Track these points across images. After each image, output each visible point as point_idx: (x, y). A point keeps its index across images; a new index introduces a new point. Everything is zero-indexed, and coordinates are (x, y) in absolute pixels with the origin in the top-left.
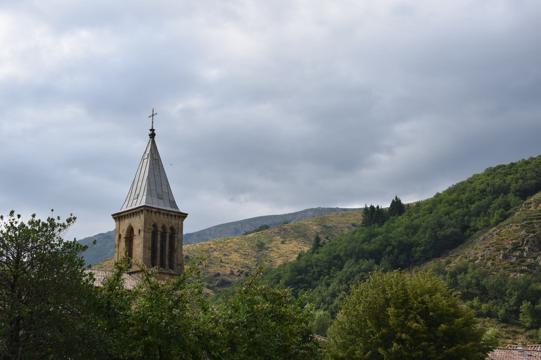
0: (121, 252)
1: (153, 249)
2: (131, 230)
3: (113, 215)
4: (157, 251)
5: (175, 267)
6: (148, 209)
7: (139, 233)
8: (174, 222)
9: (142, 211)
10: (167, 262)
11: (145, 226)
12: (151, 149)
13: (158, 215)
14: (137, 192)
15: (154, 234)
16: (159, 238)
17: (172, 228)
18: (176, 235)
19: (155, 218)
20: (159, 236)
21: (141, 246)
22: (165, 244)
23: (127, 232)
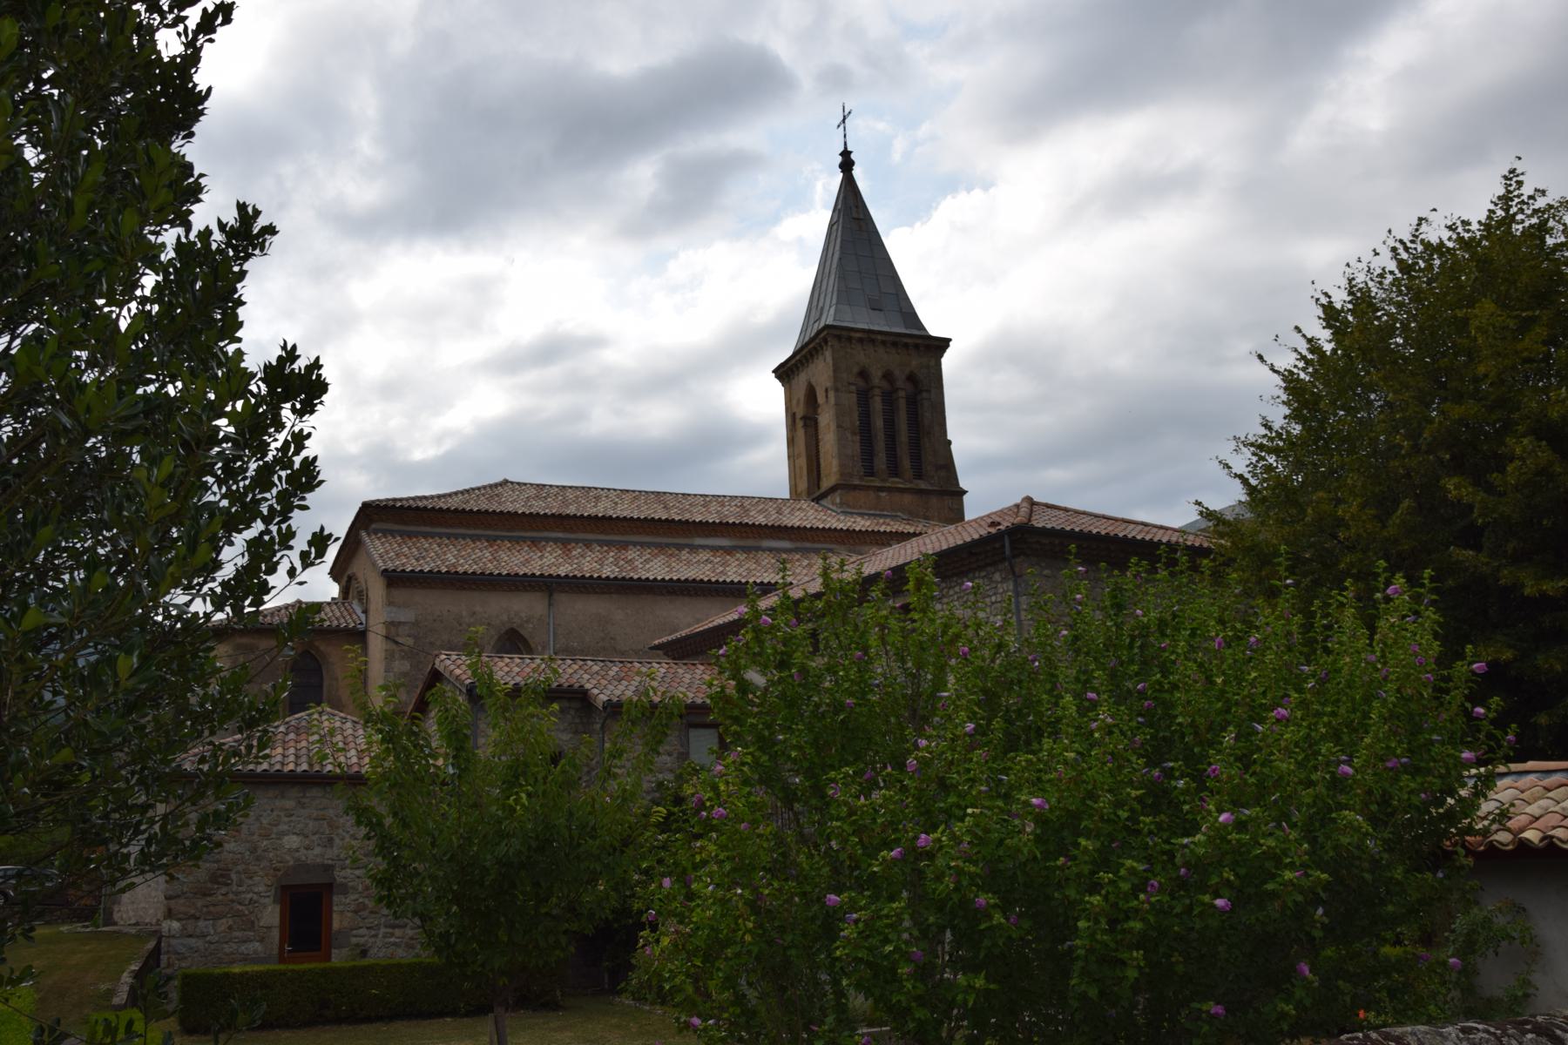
0: (799, 456)
6: (837, 332)
8: (915, 362)
15: (864, 397)
16: (879, 423)
17: (911, 378)
21: (833, 426)
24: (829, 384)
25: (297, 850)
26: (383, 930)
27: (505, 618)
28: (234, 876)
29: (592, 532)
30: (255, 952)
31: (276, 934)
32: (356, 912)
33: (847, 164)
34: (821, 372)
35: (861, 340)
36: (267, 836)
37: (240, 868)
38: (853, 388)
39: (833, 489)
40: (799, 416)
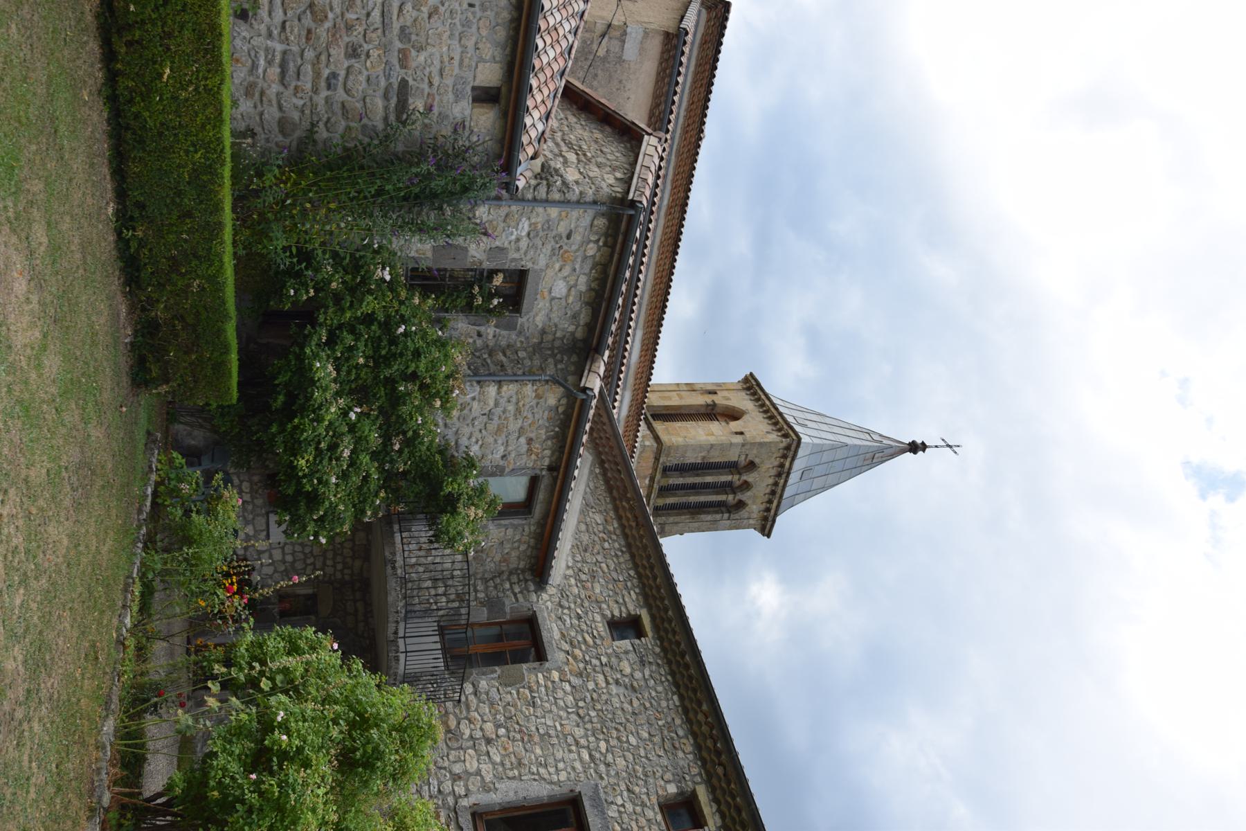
0: (681, 397)
2: (733, 415)
3: (751, 374)
4: (698, 475)
6: (793, 448)
7: (736, 433)
8: (755, 509)
9: (786, 436)
10: (671, 500)
11: (753, 444)
13: (773, 472)
14: (810, 424)
15: (732, 467)
17: (741, 505)
18: (726, 515)
19: (768, 466)
20: (729, 478)
21: (712, 440)
23: (727, 407)
24: (748, 435)
26: (279, 48)
29: (664, 234)
33: (914, 448)
34: (755, 427)
35: (782, 466)
38: (743, 457)
39: (657, 438)
40: (714, 397)
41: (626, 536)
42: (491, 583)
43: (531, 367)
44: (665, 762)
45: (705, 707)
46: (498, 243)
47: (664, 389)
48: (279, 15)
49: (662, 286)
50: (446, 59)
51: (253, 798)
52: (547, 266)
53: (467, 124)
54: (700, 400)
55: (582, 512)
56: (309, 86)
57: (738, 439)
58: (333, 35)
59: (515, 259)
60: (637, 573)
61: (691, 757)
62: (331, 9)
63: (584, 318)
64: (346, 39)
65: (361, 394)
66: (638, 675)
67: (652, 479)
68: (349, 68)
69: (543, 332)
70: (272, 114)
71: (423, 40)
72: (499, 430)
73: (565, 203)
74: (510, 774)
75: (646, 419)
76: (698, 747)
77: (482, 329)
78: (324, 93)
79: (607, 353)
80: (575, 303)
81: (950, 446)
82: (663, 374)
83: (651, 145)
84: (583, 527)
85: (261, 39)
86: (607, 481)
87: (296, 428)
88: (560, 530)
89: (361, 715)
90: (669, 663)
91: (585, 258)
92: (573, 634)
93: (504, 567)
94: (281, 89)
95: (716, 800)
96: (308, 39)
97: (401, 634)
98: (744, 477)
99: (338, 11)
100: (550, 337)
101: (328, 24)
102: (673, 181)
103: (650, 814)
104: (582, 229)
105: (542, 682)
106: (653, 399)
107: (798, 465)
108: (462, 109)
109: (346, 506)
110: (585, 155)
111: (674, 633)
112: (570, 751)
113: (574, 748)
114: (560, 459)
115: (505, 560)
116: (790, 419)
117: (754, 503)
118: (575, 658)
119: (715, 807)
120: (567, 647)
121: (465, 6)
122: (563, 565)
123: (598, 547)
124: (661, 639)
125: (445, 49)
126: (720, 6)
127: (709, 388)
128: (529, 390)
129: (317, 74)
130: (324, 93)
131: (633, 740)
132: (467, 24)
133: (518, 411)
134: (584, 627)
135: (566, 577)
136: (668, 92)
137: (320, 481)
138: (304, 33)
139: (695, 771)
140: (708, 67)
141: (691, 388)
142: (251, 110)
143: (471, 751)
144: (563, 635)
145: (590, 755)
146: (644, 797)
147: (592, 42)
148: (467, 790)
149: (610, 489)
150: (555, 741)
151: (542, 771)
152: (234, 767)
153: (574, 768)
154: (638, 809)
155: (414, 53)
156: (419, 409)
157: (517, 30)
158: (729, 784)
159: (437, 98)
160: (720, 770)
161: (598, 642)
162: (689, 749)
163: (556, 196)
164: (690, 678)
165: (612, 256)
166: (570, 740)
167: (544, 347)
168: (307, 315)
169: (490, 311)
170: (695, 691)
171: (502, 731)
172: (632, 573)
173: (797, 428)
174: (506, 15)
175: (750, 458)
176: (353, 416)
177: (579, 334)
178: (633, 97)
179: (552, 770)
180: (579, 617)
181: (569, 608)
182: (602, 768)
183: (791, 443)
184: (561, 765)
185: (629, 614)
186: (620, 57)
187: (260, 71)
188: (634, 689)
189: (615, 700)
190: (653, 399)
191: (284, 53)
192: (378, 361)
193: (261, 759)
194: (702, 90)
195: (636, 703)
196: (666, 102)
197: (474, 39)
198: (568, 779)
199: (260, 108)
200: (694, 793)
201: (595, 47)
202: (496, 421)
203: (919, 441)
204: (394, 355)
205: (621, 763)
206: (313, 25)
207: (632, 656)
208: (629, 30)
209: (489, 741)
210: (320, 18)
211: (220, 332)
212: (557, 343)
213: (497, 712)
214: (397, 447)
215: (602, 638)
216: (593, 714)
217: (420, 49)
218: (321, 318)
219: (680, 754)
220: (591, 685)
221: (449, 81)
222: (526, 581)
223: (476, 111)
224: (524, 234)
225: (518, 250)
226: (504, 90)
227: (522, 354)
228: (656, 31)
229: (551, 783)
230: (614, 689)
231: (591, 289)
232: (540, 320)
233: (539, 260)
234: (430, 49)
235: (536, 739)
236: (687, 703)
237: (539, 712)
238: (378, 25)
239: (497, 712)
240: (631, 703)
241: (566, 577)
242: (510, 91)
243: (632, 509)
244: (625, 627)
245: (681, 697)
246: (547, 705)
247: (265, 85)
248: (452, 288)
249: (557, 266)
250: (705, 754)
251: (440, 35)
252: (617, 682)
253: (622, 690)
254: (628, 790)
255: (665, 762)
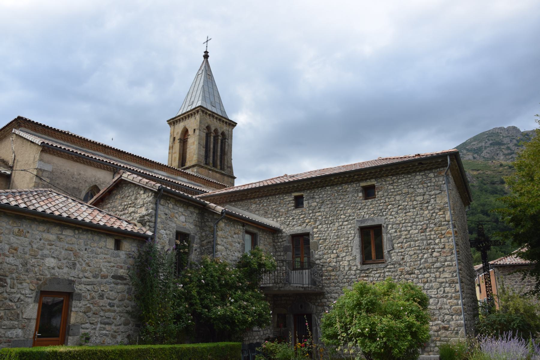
0: (175, 153)
1: (207, 147)
2: (185, 132)
3: (168, 121)
4: (210, 150)
5: (226, 168)
6: (203, 109)
7: (194, 132)
8: (225, 128)
9: (198, 112)
11: (200, 126)
12: (205, 66)
13: (212, 118)
14: (191, 101)
15: (208, 135)
17: (223, 134)
18: (227, 140)
19: (209, 121)
21: (196, 143)
22: (217, 146)
23: (182, 134)
24: (196, 128)
25: (53, 268)
26: (99, 325)
27: (93, 179)
28: (9, 281)
29: (116, 156)
30: (17, 336)
31: (33, 324)
32: (85, 313)
33: (206, 56)
34: (193, 124)
35: (210, 115)
36: (35, 256)
37: (14, 275)
38: (205, 131)
39: (193, 166)
41: (262, 197)
42: (278, 249)
43: (209, 231)
44: (350, 195)
45: (333, 179)
46: (167, 242)
47: (171, 159)
48: (88, 325)
49: (137, 159)
50: (105, 260)
51: (385, 339)
52: (175, 223)
53: (128, 253)
54: (177, 145)
55: (251, 212)
56: (113, 314)
57: (197, 132)
58: (95, 304)
59: (172, 236)
60: (277, 194)
61: (350, 186)
62: (86, 305)
63: (192, 209)
64: (97, 299)
65: (223, 298)
66: (317, 200)
67: (210, 170)
68: (107, 298)
69: (196, 225)
70: (122, 328)
71: (97, 269)
72: (231, 245)
73: (156, 216)
74: (350, 250)
75: (184, 169)
76: (346, 183)
77: (194, 249)
78: (115, 308)
79: (206, 202)
80: (187, 213)
81: (207, 41)
82: (164, 160)
83: (127, 176)
84: (257, 212)
85: (96, 332)
86: (238, 201)
87: (238, 321)
88: (263, 224)
89: (356, 306)
90: (314, 188)
91: (173, 208)
92: (300, 222)
93: (272, 244)
94: (113, 324)
95: (366, 180)
96: (97, 314)
97: (302, 286)
98: (212, 131)
99: (87, 302)
100: (198, 223)
101: (92, 307)
102: (94, 150)
103: (369, 203)
104: (166, 209)
105: (317, 235)
106: (175, 164)
107: (209, 108)
108: (122, 254)
109: (262, 304)
110: (130, 204)
111: (303, 185)
112: (344, 228)
113: (343, 227)
114: (241, 222)
115: (269, 244)
116: (189, 109)
117: (223, 128)
118: (309, 222)
119: (368, 180)
120: (305, 224)
121: (86, 252)
122: (272, 222)
123: (266, 208)
124: (304, 190)
125: (101, 261)
126: (19, 121)
127: (172, 140)
128: (220, 233)
129: (109, 311)
130: (115, 308)
131: (342, 206)
132: (92, 252)
133: (226, 238)
134: (297, 217)
135: (277, 221)
136: (67, 153)
137: (255, 313)
138: (95, 316)
139: (355, 185)
140: (47, 130)
141: (171, 148)
142: (121, 336)
143: (341, 263)
144: (300, 225)
145: (346, 221)
146: (362, 205)
147: (43, 184)
148: (355, 265)
149: (242, 200)
150: (340, 233)
151: (350, 239)
152: (374, 345)
153: (350, 228)
154: (366, 207)
155: (102, 273)
156: (230, 276)
157: (95, 232)
158: (361, 175)
159: (118, 264)
160: (356, 177)
161: (303, 213)
162: (347, 186)
163: (153, 219)
164: (321, 182)
165: (173, 198)
166: (340, 228)
167: (201, 225)
168: (197, 316)
169: (189, 245)
170: (326, 181)
171: (334, 251)
172: (277, 196)
173: (194, 107)
174: (90, 236)
175: (205, 128)
176: (233, 300)
177: (197, 211)
178: (68, 168)
179: (350, 235)
180: (293, 219)
181: (290, 222)
182: (351, 218)
183: (201, 110)
184: (349, 232)
185: (293, 200)
186: (51, 172)
187: (107, 332)
188: (323, 202)
189: (326, 210)
190: (175, 164)
191: (101, 323)
192: (213, 290)
193: (372, 337)
194: (57, 133)
195: (328, 203)
196: (71, 154)
197: (98, 249)
198: (354, 230)
199: (120, 333)
200: (363, 187)
201: (45, 183)
202: (228, 246)
203: (204, 54)
204: (212, 285)
205: (349, 211)
206: (92, 312)
207: (310, 201)
208: (39, 168)
209: (338, 257)
210: (89, 309)
211: (223, 348)
212: (200, 220)
213: (327, 252)
214: (240, 284)
215: (302, 211)
216: (331, 218)
217: (101, 270)
218: (199, 311)
219: (348, 189)
220: (320, 218)
221: (113, 259)
222: (277, 236)
223: (123, 249)
224: (165, 232)
225: (170, 234)
226: (116, 238)
227: (203, 234)
228: (40, 156)
229: (355, 236)
230: (322, 210)
231: (183, 207)
232: (192, 227)
233: (173, 226)
234: (101, 266)
235: (338, 240)
236: (330, 184)
237: (328, 237)
238: (92, 286)
239: (327, 252)
240: (328, 204)
241: (277, 221)
242: (117, 235)
243: (252, 193)
244: (299, 202)
245: (328, 186)
246: (326, 234)
247: (112, 331)
248: (181, 260)
249: (176, 219)
250: (349, 181)
251: (96, 262)
252: (320, 208)
253: (322, 207)
254: (359, 210)
255: (350, 195)
